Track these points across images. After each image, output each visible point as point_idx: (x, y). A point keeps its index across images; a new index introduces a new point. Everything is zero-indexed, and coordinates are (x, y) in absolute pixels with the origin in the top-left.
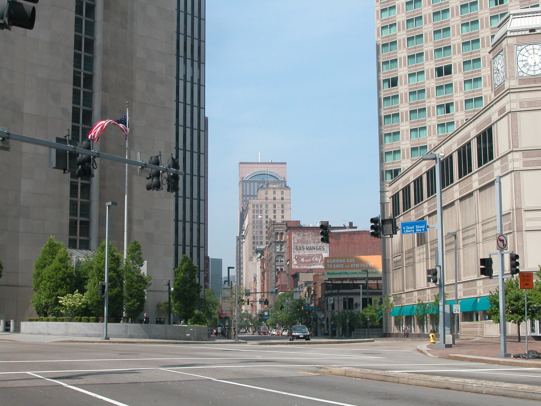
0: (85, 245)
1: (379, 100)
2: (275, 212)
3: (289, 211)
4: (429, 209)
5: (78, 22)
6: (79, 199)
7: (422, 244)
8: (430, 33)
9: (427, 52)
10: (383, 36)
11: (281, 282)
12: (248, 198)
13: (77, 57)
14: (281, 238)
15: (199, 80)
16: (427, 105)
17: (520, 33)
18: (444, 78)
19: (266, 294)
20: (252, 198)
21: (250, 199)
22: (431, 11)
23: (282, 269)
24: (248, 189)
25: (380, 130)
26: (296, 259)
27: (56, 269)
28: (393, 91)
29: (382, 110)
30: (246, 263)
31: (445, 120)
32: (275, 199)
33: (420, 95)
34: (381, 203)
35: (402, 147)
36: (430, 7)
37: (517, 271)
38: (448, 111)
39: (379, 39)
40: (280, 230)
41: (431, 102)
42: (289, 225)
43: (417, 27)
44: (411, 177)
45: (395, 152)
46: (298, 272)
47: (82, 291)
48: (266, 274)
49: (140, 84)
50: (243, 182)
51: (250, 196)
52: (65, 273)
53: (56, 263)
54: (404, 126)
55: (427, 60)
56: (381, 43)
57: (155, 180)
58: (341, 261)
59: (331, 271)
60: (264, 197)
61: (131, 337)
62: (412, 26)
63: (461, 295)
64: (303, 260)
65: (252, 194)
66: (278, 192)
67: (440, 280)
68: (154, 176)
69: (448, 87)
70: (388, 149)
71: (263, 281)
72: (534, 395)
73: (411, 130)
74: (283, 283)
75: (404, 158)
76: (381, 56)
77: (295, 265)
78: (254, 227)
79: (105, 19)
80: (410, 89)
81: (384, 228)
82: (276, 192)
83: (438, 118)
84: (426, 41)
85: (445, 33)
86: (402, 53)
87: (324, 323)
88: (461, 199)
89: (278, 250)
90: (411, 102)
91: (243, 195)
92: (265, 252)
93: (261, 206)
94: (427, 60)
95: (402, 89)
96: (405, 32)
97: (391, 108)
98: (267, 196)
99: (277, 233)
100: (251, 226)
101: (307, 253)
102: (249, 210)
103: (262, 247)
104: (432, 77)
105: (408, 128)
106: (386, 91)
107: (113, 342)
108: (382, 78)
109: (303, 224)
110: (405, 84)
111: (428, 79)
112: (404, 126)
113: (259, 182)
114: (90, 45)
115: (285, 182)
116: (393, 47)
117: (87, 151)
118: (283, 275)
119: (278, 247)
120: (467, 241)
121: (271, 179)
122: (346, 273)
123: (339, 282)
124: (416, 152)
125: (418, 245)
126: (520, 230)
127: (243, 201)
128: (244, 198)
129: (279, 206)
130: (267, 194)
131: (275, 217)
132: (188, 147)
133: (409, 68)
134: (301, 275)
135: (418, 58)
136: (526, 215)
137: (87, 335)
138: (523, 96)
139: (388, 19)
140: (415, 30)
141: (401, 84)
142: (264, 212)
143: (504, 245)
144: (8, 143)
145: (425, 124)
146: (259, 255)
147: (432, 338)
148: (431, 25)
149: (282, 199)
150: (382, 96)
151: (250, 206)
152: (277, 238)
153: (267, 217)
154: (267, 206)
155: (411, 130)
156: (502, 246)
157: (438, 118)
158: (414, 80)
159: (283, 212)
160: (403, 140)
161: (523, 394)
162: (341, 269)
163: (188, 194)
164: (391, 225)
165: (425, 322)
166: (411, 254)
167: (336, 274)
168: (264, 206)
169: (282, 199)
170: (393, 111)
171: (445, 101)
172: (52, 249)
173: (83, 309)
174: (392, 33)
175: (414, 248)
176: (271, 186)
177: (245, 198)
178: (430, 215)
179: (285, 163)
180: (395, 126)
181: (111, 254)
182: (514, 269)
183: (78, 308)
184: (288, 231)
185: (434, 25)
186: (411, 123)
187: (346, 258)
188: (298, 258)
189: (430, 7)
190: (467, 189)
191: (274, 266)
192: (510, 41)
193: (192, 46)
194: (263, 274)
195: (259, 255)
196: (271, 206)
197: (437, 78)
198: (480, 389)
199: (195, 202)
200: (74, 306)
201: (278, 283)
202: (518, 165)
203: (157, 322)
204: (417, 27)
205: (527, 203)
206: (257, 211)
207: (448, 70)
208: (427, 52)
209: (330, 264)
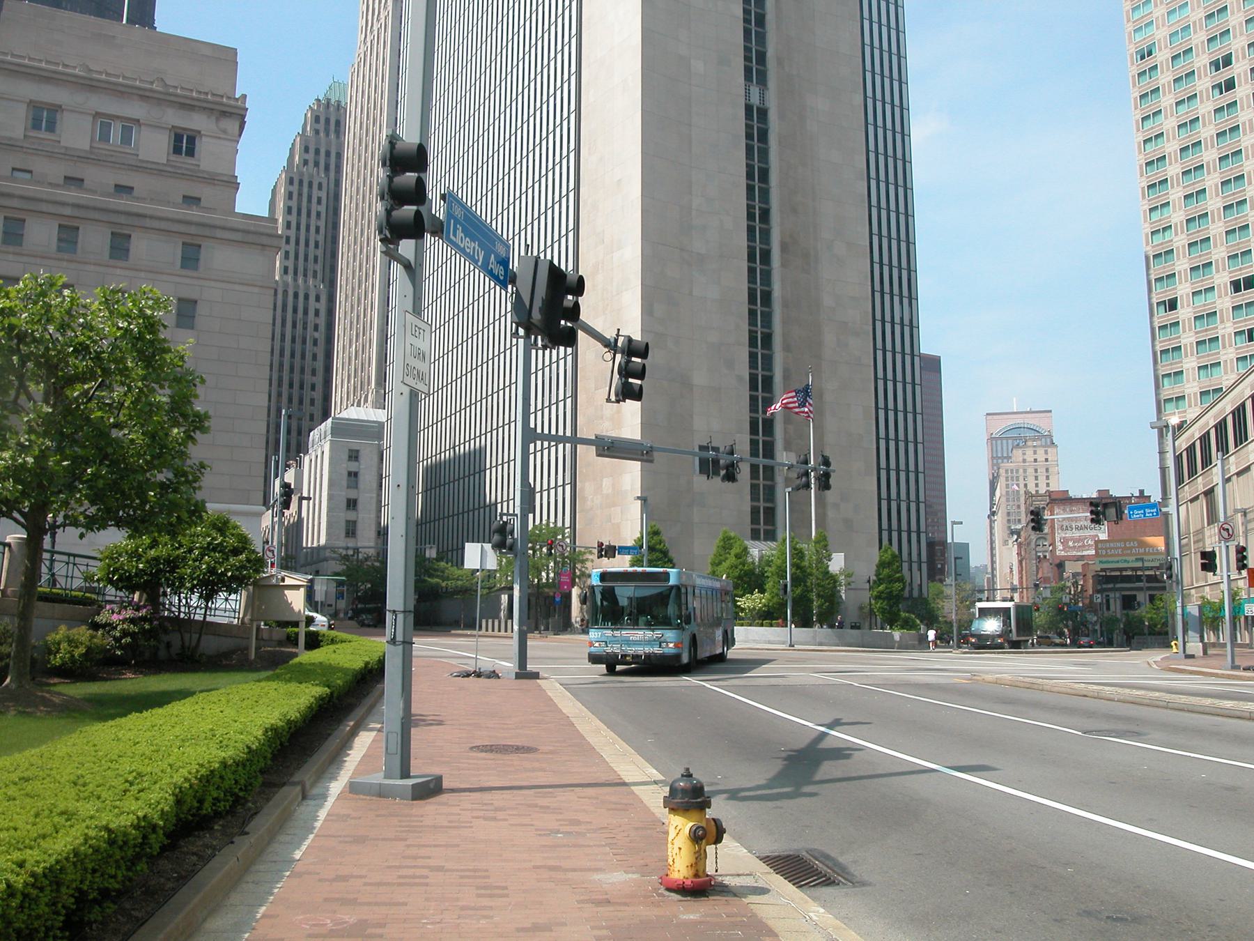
0: (770, 536)
1: (1153, 329)
2: (1036, 478)
3: (1057, 476)
5: (751, 271)
7: (1213, 523)
8: (1220, 234)
9: (1217, 261)
10: (1154, 244)
11: (1043, 573)
12: (1000, 461)
13: (752, 313)
15: (911, 321)
16: (1220, 333)
18: (1243, 295)
19: (1025, 590)
20: (1005, 460)
21: (1002, 462)
22: (1221, 205)
23: (1045, 557)
24: (999, 448)
25: (1155, 370)
26: (1062, 543)
27: (732, 567)
28: (1172, 316)
29: (1157, 343)
30: (999, 549)
31: (1247, 351)
32: (1035, 460)
33: (1210, 319)
34: (1160, 468)
35: (1187, 392)
36: (1219, 199)
37: (1244, 566)
39: (1149, 248)
42: (1053, 497)
43: (1202, 228)
44: (1195, 433)
45: (1178, 399)
46: (1063, 559)
47: (762, 591)
49: (829, 338)
50: (992, 439)
51: (1003, 458)
52: (741, 570)
53: (732, 560)
54: (1189, 363)
55: (1218, 271)
56: (1151, 254)
57: (804, 479)
58: (1118, 545)
60: (1021, 459)
61: (821, 644)
62: (1194, 227)
64: (1071, 544)
65: (1005, 455)
66: (1041, 451)
67: (1177, 576)
68: (802, 475)
69: (1249, 307)
70: (1167, 395)
71: (1021, 572)
72: (1157, 702)
73: (1199, 368)
74: (1045, 575)
75: (1190, 406)
76: (1151, 271)
78: (1008, 500)
79: (783, 265)
80: (1195, 313)
81: (1107, 514)
82: (1038, 452)
83: (1237, 349)
84: (1215, 246)
85: (1242, 233)
86: (1181, 264)
87: (1096, 628)
90: (1198, 330)
91: (992, 457)
92: (1022, 533)
93: (1017, 471)
94: (1218, 271)
95: (1184, 313)
96: (1184, 236)
97: (1170, 340)
98: (1025, 457)
100: (1003, 499)
101: (1077, 534)
102: (1001, 478)
103: (1019, 527)
104: (1226, 294)
105: (1195, 365)
106: (1161, 317)
107: (799, 650)
108: (1155, 301)
109: (1071, 494)
110: (1188, 306)
111: (1220, 297)
112: (1189, 363)
113: (1015, 439)
114: (767, 298)
115: (1050, 436)
116: (1168, 257)
117: (730, 457)
118: (1045, 565)
121: (1029, 434)
122: (1125, 561)
123: (1118, 573)
124: (1207, 397)
125: (1208, 525)
127: (993, 465)
128: (995, 461)
129: (1042, 471)
130: (1024, 454)
131: (1037, 485)
132: (900, 407)
133: (1192, 284)
134: (1067, 563)
135: (1205, 270)
137: (770, 642)
139: (1160, 220)
140: (1198, 232)
141: (1182, 307)
142: (1021, 479)
143: (1229, 534)
144: (652, 456)
145: (1219, 358)
147: (1174, 647)
148: (1221, 224)
149: (1047, 460)
150: (1156, 325)
151: (1002, 471)
153: (1026, 485)
154: (1025, 471)
155: (1199, 368)
156: (1226, 536)
157: (1237, 349)
158: (1200, 300)
159: (1048, 478)
160: (1188, 381)
161: (1148, 701)
162: (1118, 555)
163: (902, 466)
164: (1114, 509)
165: (1221, 628)
166: (1200, 536)
167: (1112, 562)
168: (1021, 471)
169: (1047, 460)
170: (1173, 344)
171: (1246, 326)
172: (727, 543)
173: (764, 611)
174: (1166, 239)
175: (1203, 528)
176: (1029, 443)
177: (996, 460)
179: (1050, 411)
180: (1176, 363)
181: (793, 548)
182: (1241, 564)
183: (759, 610)
184: (1049, 505)
185: (1225, 222)
186: (1198, 358)
187: (1125, 541)
188: (1065, 542)
189: (1219, 199)
191: (1034, 552)
193: (900, 278)
194: (1020, 562)
195: (1015, 537)
196: (1031, 471)
197: (1234, 295)
198: (1112, 696)
199: (912, 476)
200: (754, 608)
201: (1039, 576)
203: (852, 627)
204: (1202, 228)
206: (1012, 477)
208: (1217, 261)
209: (1102, 549)
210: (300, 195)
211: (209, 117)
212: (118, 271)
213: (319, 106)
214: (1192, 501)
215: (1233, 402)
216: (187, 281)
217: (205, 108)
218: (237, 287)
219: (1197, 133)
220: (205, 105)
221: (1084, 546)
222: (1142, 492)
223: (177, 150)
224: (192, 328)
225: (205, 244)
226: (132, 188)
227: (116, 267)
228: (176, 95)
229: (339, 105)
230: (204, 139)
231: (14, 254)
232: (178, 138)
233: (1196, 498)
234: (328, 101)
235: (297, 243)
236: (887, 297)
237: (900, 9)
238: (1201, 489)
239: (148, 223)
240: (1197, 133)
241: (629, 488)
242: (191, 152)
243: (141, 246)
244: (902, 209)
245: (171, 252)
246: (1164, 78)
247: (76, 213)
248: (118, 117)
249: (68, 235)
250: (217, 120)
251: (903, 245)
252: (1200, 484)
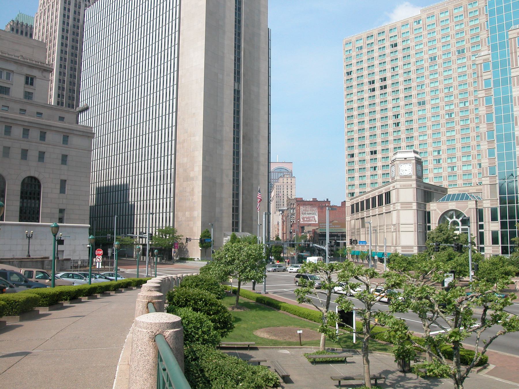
4: (366, 215)
6: (235, 213)
14: (293, 206)
17: (401, 159)
32: (287, 182)
35: (355, 184)
38: (375, 170)
40: (293, 202)
41: (368, 165)
48: (285, 223)
59: (321, 229)
62: (359, 72)
63: (378, 250)
66: (289, 179)
77: (302, 222)
88: (379, 214)
89: (292, 212)
93: (281, 186)
99: (291, 204)
100: (275, 197)
101: (308, 216)
105: (358, 175)
113: (278, 172)
115: (291, 172)
119: (292, 211)
120: (381, 231)
126: (399, 231)
129: (289, 186)
136: (401, 226)
138: (401, 183)
142: (282, 189)
146: (281, 212)
149: (291, 183)
152: (291, 206)
154: (283, 186)
158: (361, 155)
159: (291, 189)
168: (282, 186)
169: (291, 183)
176: (285, 176)
178: (367, 217)
188: (303, 218)
190: (381, 211)
192: (398, 162)
194: (283, 222)
196: (285, 186)
202: (399, 208)
205: (401, 222)
207: (375, 152)
211: (39, 71)
212: (43, 145)
213: (13, 23)
214: (356, 219)
215: (372, 194)
216: (65, 148)
217: (38, 68)
218: (81, 151)
220: (38, 67)
221: (310, 220)
222: (327, 199)
223: (27, 83)
224: (66, 164)
225: (70, 136)
226: (42, 113)
227: (42, 144)
228: (28, 62)
229: (22, 24)
230: (37, 79)
231: (9, 139)
232: (27, 78)
233: (358, 219)
234: (18, 21)
238: (360, 217)
239: (52, 128)
241: (196, 216)
242: (32, 84)
243: (49, 136)
245: (59, 138)
246: (354, 83)
247: (29, 124)
248: (5, 69)
249: (26, 132)
250: (42, 72)
252: (360, 215)
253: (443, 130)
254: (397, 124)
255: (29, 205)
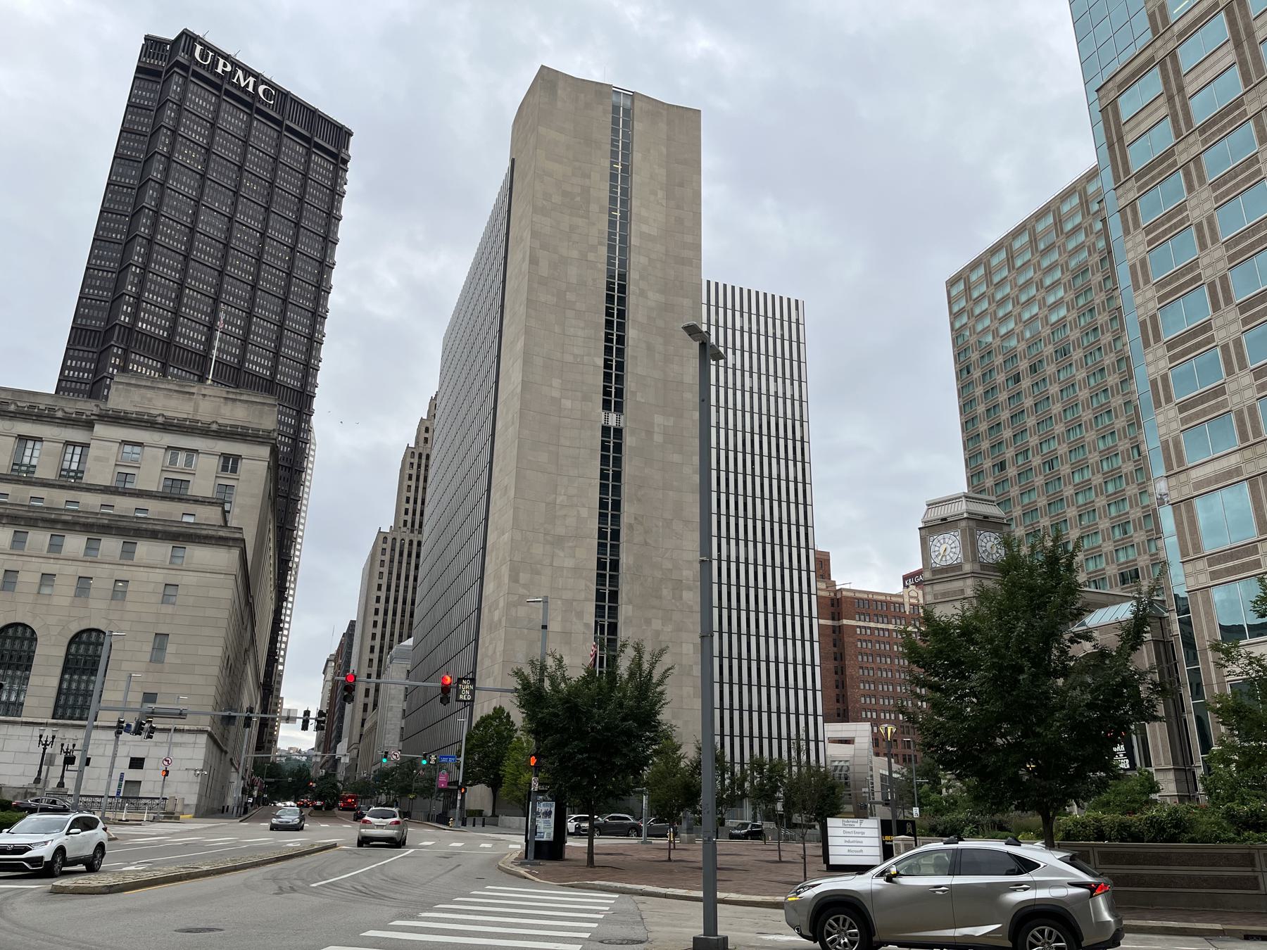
15: (802, 438)
210: (417, 488)
219: (1130, 537)
223: (225, 469)
235: (415, 502)
236: (784, 505)
237: (803, 365)
240: (1130, 537)
242: (234, 470)
244: (794, 338)
251: (801, 507)
253: (1090, 436)
254: (1002, 466)
255: (74, 686)
